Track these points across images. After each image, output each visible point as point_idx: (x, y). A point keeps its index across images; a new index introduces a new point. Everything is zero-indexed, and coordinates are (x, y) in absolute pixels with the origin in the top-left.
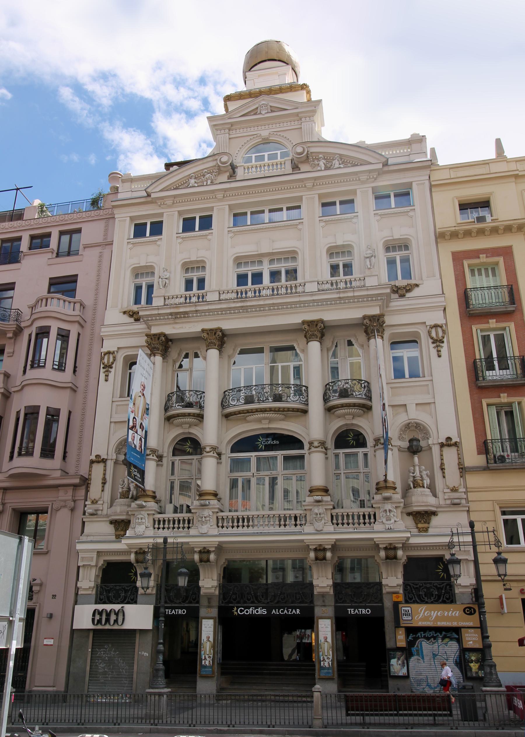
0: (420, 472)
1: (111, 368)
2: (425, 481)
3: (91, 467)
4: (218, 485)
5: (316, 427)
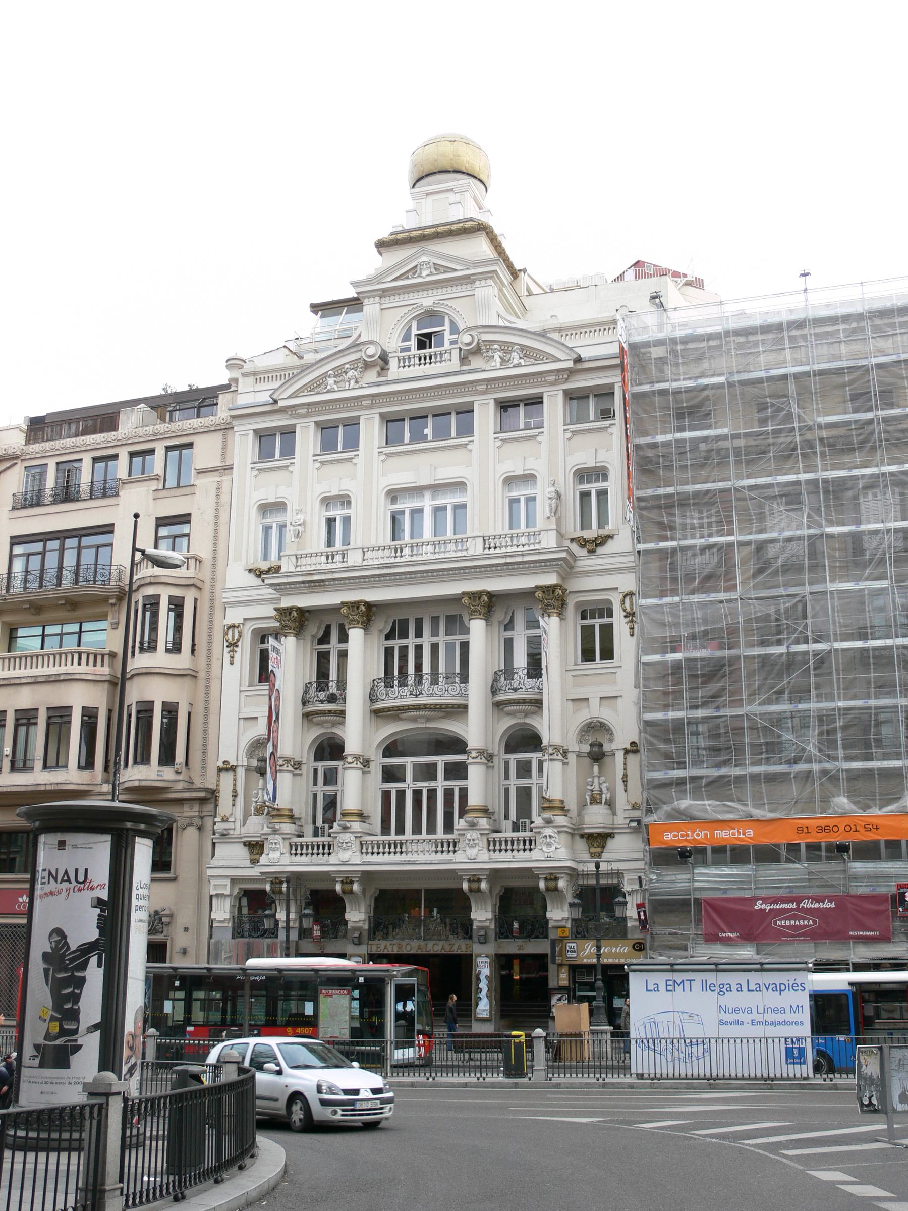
0: (600, 784)
1: (237, 646)
2: (604, 796)
3: (219, 776)
4: (363, 799)
5: (476, 729)
